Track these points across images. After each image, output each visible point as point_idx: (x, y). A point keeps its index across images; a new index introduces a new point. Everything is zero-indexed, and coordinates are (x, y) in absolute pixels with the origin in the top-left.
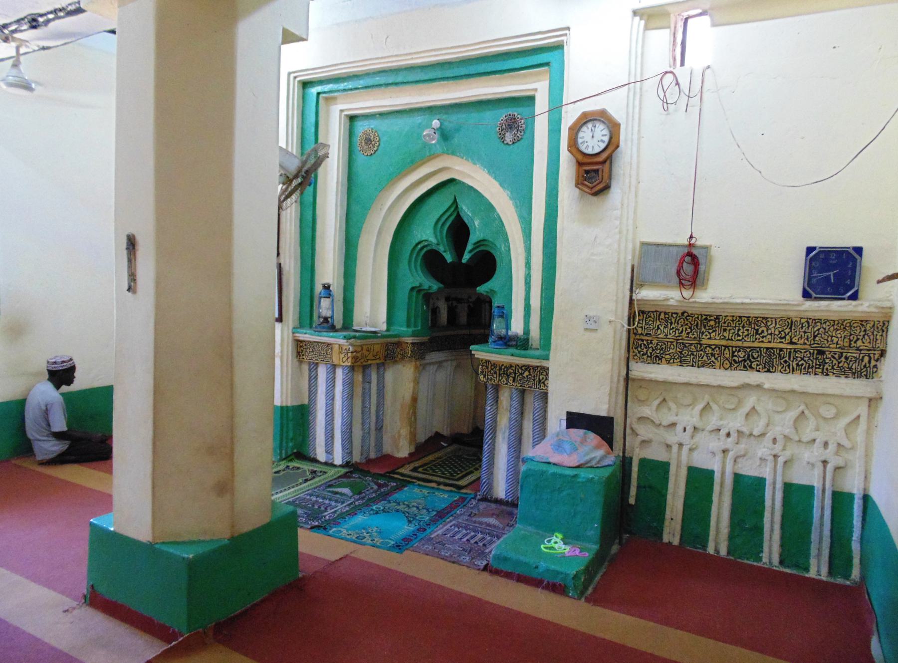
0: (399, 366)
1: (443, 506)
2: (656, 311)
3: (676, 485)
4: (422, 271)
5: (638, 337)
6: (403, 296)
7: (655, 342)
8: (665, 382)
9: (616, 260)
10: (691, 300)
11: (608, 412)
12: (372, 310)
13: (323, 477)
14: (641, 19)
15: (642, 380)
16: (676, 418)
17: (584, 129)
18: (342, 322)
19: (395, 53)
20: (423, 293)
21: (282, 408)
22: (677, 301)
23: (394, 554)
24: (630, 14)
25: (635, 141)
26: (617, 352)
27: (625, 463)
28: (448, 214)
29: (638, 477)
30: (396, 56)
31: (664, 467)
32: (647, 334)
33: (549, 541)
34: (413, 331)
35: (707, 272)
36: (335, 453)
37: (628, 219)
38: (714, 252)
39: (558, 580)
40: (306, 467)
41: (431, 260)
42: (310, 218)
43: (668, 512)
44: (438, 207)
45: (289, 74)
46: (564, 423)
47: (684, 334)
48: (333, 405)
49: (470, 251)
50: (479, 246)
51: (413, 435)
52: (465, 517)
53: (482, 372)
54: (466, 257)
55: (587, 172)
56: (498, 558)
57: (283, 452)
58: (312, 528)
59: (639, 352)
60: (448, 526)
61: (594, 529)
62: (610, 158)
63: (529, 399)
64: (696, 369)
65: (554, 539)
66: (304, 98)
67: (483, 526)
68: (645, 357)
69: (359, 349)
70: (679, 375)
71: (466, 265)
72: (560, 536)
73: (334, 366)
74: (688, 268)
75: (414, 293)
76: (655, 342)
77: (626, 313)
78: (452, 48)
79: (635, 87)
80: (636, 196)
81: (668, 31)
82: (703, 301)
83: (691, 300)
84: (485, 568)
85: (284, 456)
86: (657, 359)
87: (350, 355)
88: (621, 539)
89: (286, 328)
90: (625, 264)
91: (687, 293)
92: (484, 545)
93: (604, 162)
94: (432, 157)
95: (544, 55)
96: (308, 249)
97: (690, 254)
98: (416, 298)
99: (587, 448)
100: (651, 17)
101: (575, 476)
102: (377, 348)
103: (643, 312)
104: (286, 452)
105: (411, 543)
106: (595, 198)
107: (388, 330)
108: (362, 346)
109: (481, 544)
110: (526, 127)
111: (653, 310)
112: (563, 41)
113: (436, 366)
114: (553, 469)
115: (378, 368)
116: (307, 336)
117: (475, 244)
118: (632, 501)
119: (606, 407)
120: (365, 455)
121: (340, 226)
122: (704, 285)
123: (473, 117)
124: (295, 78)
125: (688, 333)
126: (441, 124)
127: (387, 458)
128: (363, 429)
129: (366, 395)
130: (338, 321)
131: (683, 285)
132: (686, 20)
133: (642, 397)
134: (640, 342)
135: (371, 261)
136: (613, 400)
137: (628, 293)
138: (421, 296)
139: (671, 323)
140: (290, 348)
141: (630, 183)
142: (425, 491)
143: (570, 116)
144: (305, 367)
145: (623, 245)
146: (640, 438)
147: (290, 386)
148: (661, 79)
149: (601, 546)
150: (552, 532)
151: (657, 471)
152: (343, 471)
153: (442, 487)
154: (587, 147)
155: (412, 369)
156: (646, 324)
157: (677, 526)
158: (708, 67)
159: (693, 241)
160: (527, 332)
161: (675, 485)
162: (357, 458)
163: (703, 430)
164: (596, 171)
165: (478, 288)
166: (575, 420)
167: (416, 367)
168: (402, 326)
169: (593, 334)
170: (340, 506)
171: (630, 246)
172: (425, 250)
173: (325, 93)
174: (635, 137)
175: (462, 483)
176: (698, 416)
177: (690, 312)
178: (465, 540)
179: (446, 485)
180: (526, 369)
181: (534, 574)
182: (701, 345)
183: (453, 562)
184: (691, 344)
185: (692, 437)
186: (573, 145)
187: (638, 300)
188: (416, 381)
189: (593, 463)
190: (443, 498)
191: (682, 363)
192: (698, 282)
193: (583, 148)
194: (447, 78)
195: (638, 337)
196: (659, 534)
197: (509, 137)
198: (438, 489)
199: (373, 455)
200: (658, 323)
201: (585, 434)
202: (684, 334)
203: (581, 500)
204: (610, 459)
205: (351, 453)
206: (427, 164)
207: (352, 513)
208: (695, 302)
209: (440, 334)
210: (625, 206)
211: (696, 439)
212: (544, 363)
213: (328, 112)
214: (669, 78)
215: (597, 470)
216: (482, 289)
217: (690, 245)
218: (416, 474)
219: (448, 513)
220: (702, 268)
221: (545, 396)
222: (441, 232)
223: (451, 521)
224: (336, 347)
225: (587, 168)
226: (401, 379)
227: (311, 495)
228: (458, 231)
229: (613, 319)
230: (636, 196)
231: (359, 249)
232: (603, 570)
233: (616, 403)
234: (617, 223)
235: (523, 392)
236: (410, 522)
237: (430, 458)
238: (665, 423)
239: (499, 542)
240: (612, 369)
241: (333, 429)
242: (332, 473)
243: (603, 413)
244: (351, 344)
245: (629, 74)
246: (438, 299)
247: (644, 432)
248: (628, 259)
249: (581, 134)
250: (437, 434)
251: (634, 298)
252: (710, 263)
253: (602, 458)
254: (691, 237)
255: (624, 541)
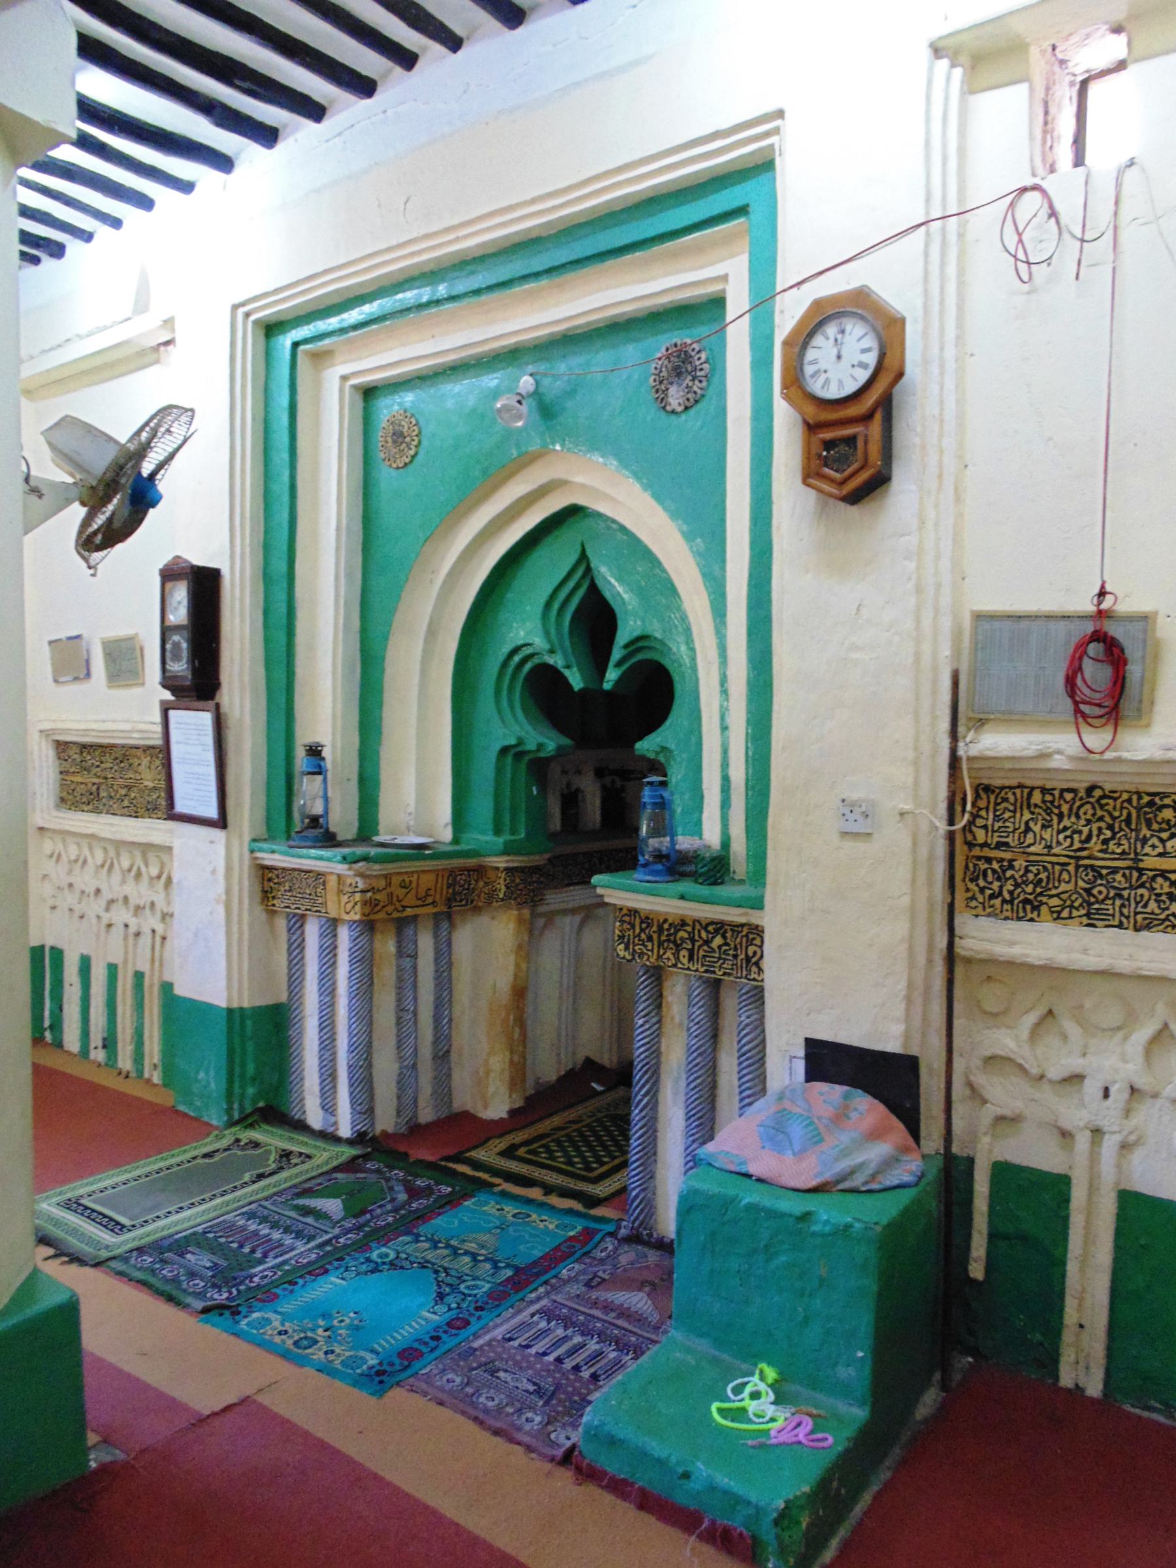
0: (484, 920)
1: (537, 1253)
2: (1021, 786)
3: (1089, 1238)
4: (524, 710)
5: (977, 852)
6: (485, 765)
7: (1020, 863)
8: (1048, 970)
9: (910, 661)
10: (1109, 755)
11: (905, 1044)
12: (421, 799)
13: (307, 1166)
14: (953, 66)
15: (991, 961)
16: (1081, 1061)
17: (818, 340)
18: (356, 824)
19: (422, 232)
20: (527, 758)
21: (230, 1011)
22: (1072, 758)
23: (362, 1399)
24: (927, 53)
25: (951, 365)
26: (923, 894)
27: (954, 1174)
28: (571, 584)
29: (991, 1207)
30: (427, 236)
31: (1055, 1188)
32: (999, 845)
33: (738, 1390)
34: (506, 843)
35: (1150, 680)
36: (340, 1111)
37: (938, 558)
38: (1165, 629)
39: (737, 1522)
40: (273, 1139)
41: (543, 688)
42: (283, 609)
43: (1070, 1304)
44: (549, 569)
45: (235, 307)
46: (800, 1067)
47: (1095, 845)
48: (332, 1005)
49: (619, 664)
50: (639, 650)
51: (518, 1072)
52: (576, 1289)
53: (621, 937)
54: (612, 675)
55: (829, 445)
56: (594, 1434)
57: (236, 1106)
58: (206, 1310)
59: (982, 890)
60: (524, 1316)
61: (855, 1364)
62: (886, 404)
63: (730, 1002)
64: (1130, 933)
65: (754, 1383)
66: (268, 356)
67: (610, 1317)
68: (997, 902)
69: (382, 883)
70: (1085, 951)
71: (608, 694)
72: (771, 1374)
73: (334, 922)
74: (1096, 673)
75: (509, 759)
76: (1020, 863)
77: (943, 793)
78: (533, 201)
79: (943, 229)
80: (958, 499)
81: (1023, 88)
82: (1140, 756)
83: (1109, 755)
84: (568, 1458)
85: (236, 1116)
86: (1026, 906)
87: (358, 897)
88: (946, 1368)
89: (236, 843)
90: (935, 668)
91: (1096, 739)
92: (595, 1377)
93: (868, 417)
94: (526, 461)
95: (728, 191)
96: (280, 675)
97: (1098, 636)
98: (515, 772)
99: (845, 1138)
100: (982, 57)
101: (806, 1217)
102: (427, 881)
103: (988, 789)
104: (242, 1108)
105: (417, 1365)
106: (853, 511)
107: (456, 840)
108: (387, 877)
109: (586, 1374)
110: (713, 369)
111: (1014, 783)
112: (772, 146)
113: (578, 919)
114: (751, 1196)
115: (436, 927)
116: (278, 858)
117: (626, 646)
118: (977, 1271)
119: (898, 1029)
120: (408, 1114)
121: (347, 618)
122: (1143, 715)
123: (600, 358)
124: (247, 315)
125: (1106, 842)
126: (537, 383)
127: (466, 1117)
128: (401, 1058)
129: (406, 983)
130: (343, 819)
131: (1084, 716)
132: (1084, 84)
133: (990, 1005)
134: (983, 866)
135: (414, 692)
136: (918, 1010)
137: (945, 743)
138: (523, 766)
139: (1061, 816)
140: (246, 883)
141: (940, 466)
142: (510, 1209)
143: (789, 313)
144: (281, 923)
145: (927, 622)
146: (990, 1111)
147: (246, 966)
148: (1012, 205)
149: (874, 1411)
150: (751, 1357)
151: (1039, 1197)
152: (349, 1152)
153: (554, 1200)
154: (827, 381)
155: (511, 926)
156: (997, 818)
157: (1095, 1343)
158: (1131, 163)
159: (1107, 604)
160: (726, 844)
161: (1086, 1235)
162: (386, 1121)
163: (1155, 1096)
164: (851, 441)
165: (638, 745)
166: (826, 1061)
167: (520, 920)
168: (483, 832)
169: (860, 846)
170: (301, 1247)
171: (946, 623)
172: (528, 667)
173: (306, 341)
174: (950, 353)
175: (601, 1190)
176: (1140, 1059)
177: (1108, 787)
178: (551, 1358)
179: (565, 1193)
180: (717, 931)
181: (681, 1498)
182: (1141, 871)
183: (497, 1432)
184: (1115, 870)
185: (1127, 1113)
186: (794, 382)
187: (971, 759)
188: (527, 950)
189: (857, 1181)
190: (547, 1228)
191: (1092, 919)
192: (1127, 707)
193: (817, 387)
194: (536, 275)
195: (977, 852)
196: (1050, 1362)
197: (675, 396)
198: (542, 1205)
199: (426, 1115)
200: (1027, 816)
201: (846, 1096)
202: (1095, 845)
203: (822, 1281)
204: (909, 1169)
205: (370, 1111)
206: (519, 477)
207: (317, 1270)
208: (1119, 760)
209: (585, 847)
210: (930, 525)
211: (1136, 1120)
212: (754, 918)
213: (318, 385)
214: (1032, 200)
215: (868, 1200)
216: (646, 746)
217: (1101, 614)
218: (513, 1166)
219: (538, 1275)
220: (1134, 670)
221: (757, 996)
222: (559, 623)
223: (539, 1299)
224: (332, 882)
225: (828, 435)
226: (489, 945)
227: (251, 1216)
228: (595, 619)
229: (907, 807)
230: (958, 499)
231: (389, 671)
232: (884, 1475)
233: (925, 1018)
234: (911, 566)
235: (715, 986)
236: (441, 1297)
237: (557, 1120)
238: (1054, 1073)
239: (632, 1366)
240: (911, 936)
241: (333, 1060)
242: (325, 1156)
243: (893, 1045)
244: (362, 875)
245: (928, 200)
246: (579, 772)
247: (1003, 1094)
248: (942, 656)
249: (811, 354)
250: (589, 1062)
251: (961, 752)
252: (1156, 657)
253: (888, 1163)
254: (1102, 594)
255: (957, 1377)
